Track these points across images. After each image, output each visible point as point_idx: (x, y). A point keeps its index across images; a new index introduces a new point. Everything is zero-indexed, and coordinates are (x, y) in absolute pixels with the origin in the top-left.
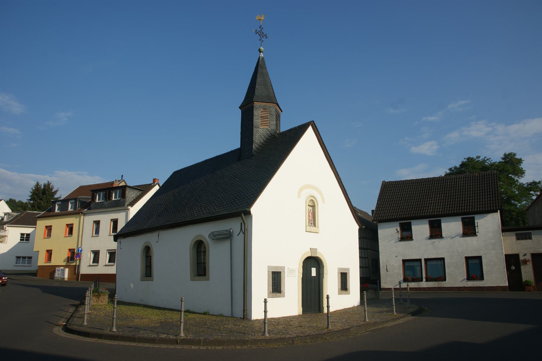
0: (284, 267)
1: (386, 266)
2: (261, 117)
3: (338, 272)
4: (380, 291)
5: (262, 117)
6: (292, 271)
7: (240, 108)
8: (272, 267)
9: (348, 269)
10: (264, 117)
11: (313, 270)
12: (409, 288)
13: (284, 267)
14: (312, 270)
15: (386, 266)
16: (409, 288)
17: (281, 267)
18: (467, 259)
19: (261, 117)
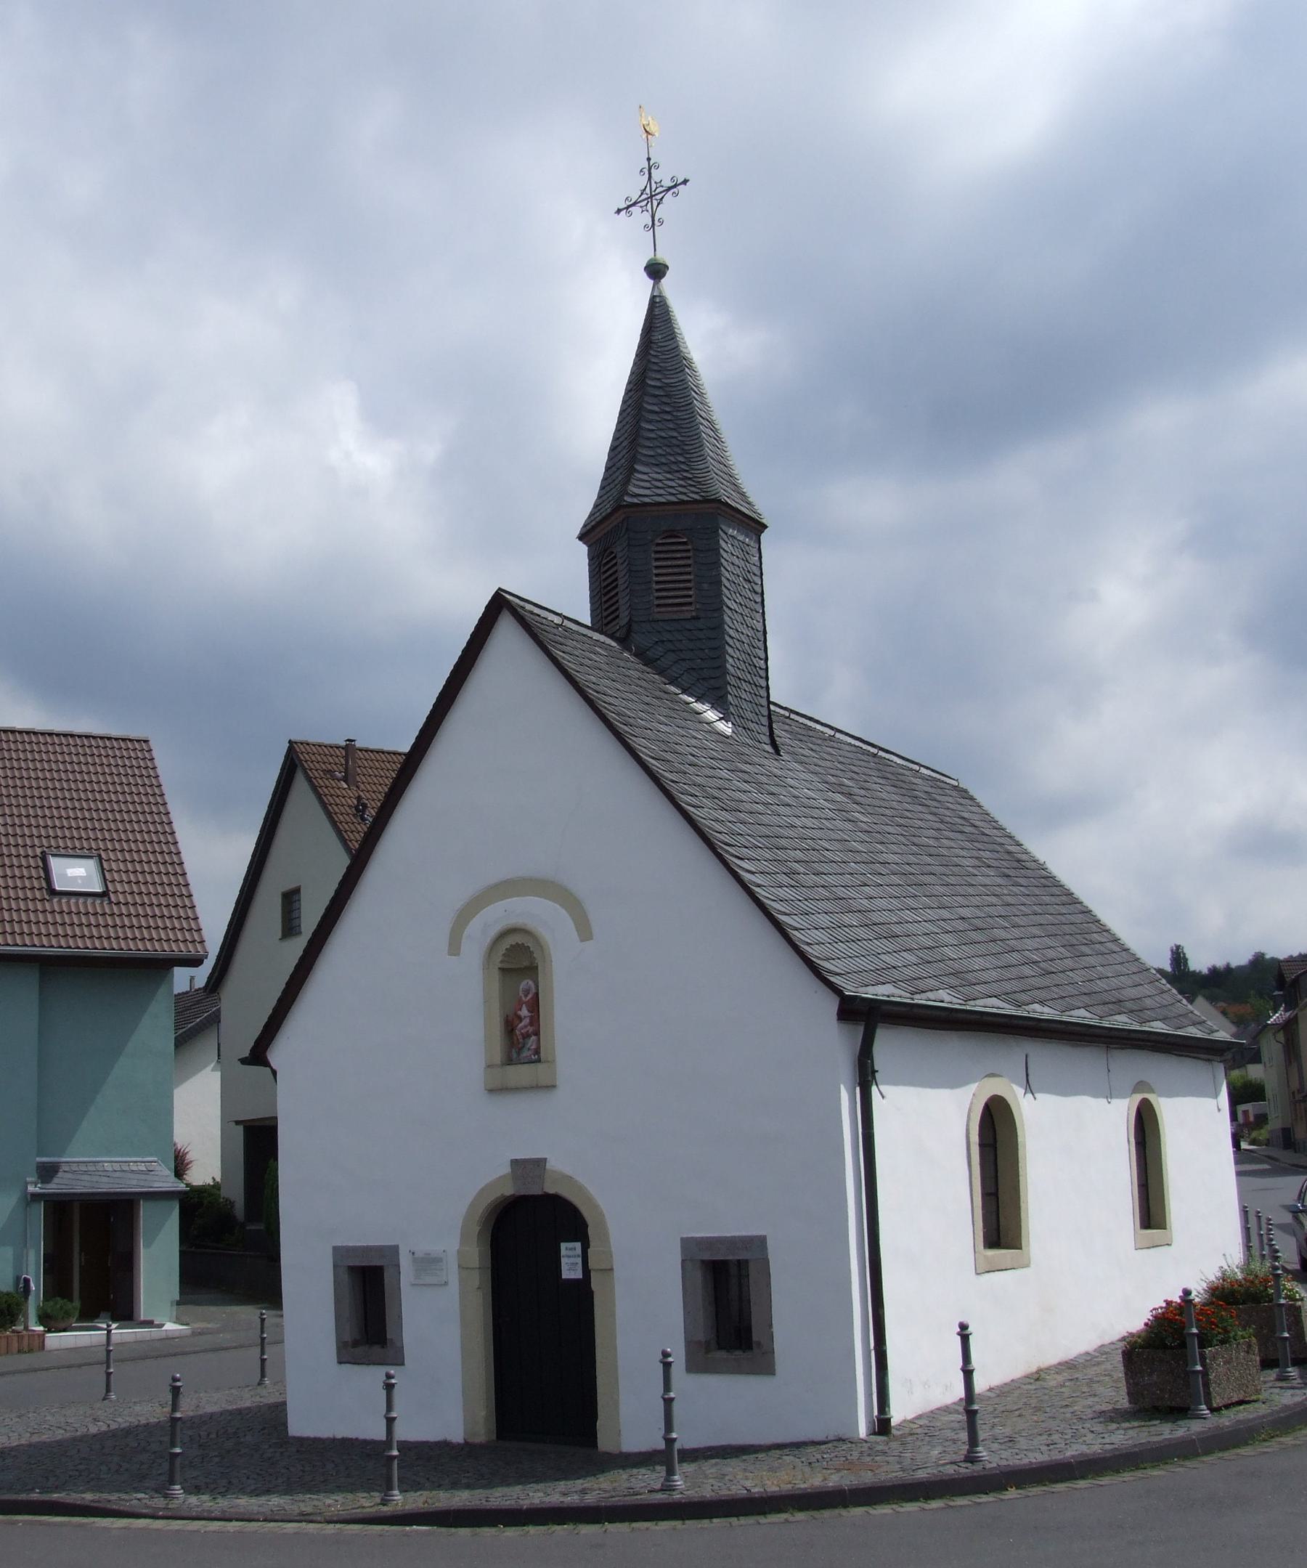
0: (394, 1250)
1: (1092, 1419)
2: (658, 556)
3: (683, 1261)
4: (1248, 1111)
5: (662, 556)
6: (427, 1263)
7: (581, 537)
8: (354, 1250)
9: (983, 1269)
10: (676, 570)
11: (570, 1253)
12: (679, 1451)
13: (394, 1250)
14: (563, 1252)
15: (1092, 1419)
16: (676, 1453)
17: (380, 1250)
18: (340, 1363)
19: (658, 556)
